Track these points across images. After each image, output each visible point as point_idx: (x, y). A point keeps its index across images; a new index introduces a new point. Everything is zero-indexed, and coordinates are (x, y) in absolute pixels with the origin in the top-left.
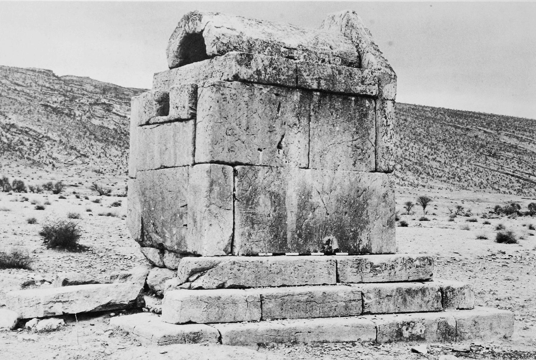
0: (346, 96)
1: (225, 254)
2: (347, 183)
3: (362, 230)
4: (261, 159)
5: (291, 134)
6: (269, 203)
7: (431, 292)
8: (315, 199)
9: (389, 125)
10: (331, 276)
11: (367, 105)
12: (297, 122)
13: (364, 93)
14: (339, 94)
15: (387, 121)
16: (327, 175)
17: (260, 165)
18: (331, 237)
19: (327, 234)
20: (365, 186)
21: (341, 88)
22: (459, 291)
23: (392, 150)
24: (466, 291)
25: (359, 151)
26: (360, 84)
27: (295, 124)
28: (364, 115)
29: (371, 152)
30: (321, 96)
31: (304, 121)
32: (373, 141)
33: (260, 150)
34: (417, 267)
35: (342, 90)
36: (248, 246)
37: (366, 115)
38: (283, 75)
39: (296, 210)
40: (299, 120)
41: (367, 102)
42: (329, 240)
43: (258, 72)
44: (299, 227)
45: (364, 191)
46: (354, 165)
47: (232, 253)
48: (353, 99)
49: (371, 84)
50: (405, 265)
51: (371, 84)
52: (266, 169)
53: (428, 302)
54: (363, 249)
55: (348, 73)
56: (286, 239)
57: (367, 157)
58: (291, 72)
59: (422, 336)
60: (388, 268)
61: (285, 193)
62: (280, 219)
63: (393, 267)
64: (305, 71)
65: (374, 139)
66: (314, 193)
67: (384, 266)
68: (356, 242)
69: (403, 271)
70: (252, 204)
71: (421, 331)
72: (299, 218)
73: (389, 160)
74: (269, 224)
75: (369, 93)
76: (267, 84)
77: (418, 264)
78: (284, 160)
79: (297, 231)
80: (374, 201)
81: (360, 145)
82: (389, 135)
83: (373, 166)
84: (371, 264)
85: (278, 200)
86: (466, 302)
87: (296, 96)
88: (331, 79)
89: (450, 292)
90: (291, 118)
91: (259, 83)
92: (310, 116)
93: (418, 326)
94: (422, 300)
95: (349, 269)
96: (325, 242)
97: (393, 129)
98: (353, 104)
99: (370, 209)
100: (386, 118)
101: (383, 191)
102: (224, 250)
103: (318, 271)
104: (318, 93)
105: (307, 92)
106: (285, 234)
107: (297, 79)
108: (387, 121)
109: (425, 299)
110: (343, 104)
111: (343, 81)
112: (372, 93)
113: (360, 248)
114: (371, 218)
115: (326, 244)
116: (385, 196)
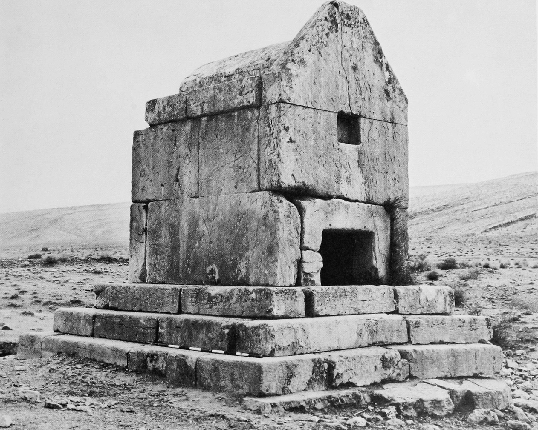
0: (228, 113)
1: (139, 281)
2: (228, 208)
3: (241, 258)
4: (163, 193)
5: (185, 165)
6: (168, 234)
7: (216, 328)
8: (203, 228)
9: (272, 134)
10: (175, 305)
11: (250, 117)
12: (189, 153)
13: (241, 105)
14: (222, 113)
15: (270, 129)
16: (211, 201)
17: (163, 200)
18: (215, 267)
19: (210, 263)
20: (246, 208)
21: (220, 106)
22: (253, 332)
23: (275, 163)
24: (261, 332)
25: (241, 171)
26: (238, 96)
27: (187, 155)
28: (247, 129)
29: (252, 170)
30: (208, 121)
31: (194, 150)
32: (255, 156)
33: (162, 185)
34: (253, 300)
35: (221, 109)
36: (153, 275)
37: (248, 129)
38: (176, 110)
39: (186, 240)
40: (190, 150)
41: (250, 113)
42: (212, 269)
43: (159, 114)
44: (188, 257)
45: (244, 214)
46: (236, 187)
47: (144, 281)
48: (236, 114)
49: (248, 92)
50: (241, 297)
51: (248, 92)
52: (167, 202)
53: (213, 339)
54: (242, 279)
55: (227, 88)
56: (178, 268)
57: (248, 176)
58: (182, 105)
59: (163, 372)
60: (224, 301)
61: (179, 223)
62: (175, 248)
63: (228, 299)
64: (192, 100)
65: (256, 153)
66: (200, 222)
67: (220, 297)
68: (235, 272)
69: (238, 305)
70: (157, 236)
71: (163, 366)
72: (190, 247)
73: (272, 175)
74: (167, 253)
75: (246, 103)
76: (166, 123)
77: (254, 297)
78: (179, 192)
79: (186, 260)
80: (254, 224)
81: (241, 164)
82: (272, 146)
83: (255, 185)
84: (209, 294)
85: (174, 230)
86: (261, 346)
87: (188, 127)
88: (213, 100)
89: (242, 331)
90: (183, 150)
91: (160, 124)
92: (199, 143)
93: (160, 360)
94: (207, 336)
95: (190, 299)
96: (208, 272)
97: (276, 138)
98: (236, 120)
99: (250, 235)
100: (269, 126)
101: (264, 211)
102: (139, 278)
103: (167, 299)
104: (206, 118)
105: (196, 119)
106: (178, 264)
107: (186, 110)
108: (270, 129)
109: (209, 335)
110: (227, 122)
111: (223, 99)
112: (249, 102)
113: (238, 279)
114: (252, 244)
115: (209, 274)
116: (266, 217)
